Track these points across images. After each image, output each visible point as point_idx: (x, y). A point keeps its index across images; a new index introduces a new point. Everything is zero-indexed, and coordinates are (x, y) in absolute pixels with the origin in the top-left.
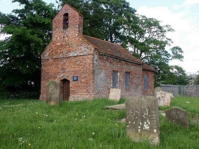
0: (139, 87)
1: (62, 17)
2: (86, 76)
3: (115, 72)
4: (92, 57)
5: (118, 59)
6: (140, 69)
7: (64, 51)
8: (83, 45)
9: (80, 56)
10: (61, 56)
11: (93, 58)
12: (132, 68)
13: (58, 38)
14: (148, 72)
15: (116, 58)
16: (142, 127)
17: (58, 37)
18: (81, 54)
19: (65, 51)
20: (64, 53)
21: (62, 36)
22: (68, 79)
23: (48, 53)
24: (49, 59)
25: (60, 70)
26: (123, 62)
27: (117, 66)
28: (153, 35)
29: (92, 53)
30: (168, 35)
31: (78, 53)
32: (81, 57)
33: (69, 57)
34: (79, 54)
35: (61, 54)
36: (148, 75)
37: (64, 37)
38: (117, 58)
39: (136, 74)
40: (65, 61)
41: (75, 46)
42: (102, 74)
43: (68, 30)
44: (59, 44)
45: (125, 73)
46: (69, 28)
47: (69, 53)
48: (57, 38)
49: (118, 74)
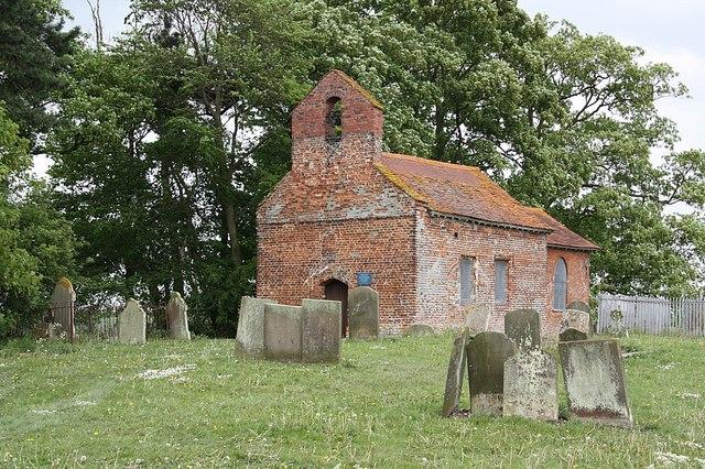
0: (537, 301)
1: (324, 106)
2: (393, 273)
3: (466, 260)
4: (411, 223)
5: (476, 223)
6: (538, 247)
7: (330, 203)
8: (386, 191)
9: (378, 219)
10: (321, 215)
11: (414, 226)
12: (516, 246)
13: (311, 166)
14: (565, 255)
15: (470, 222)
16: (524, 343)
17: (312, 163)
18: (381, 214)
19: (332, 203)
20: (329, 207)
21: (324, 161)
22: (344, 280)
23: (278, 207)
24: (282, 224)
25: (317, 254)
26: (490, 230)
27: (471, 242)
28: (600, 102)
29: (411, 213)
30: (663, 106)
31: (371, 211)
32: (381, 222)
33: (346, 220)
34: (375, 215)
35: (322, 211)
36: (569, 263)
37: (328, 165)
38: (472, 220)
39: (526, 263)
40: (332, 230)
41: (362, 192)
42: (435, 265)
43: (341, 144)
44: (313, 182)
45: (496, 260)
46: (344, 141)
47: (344, 210)
48: (307, 164)
49: (477, 265)
